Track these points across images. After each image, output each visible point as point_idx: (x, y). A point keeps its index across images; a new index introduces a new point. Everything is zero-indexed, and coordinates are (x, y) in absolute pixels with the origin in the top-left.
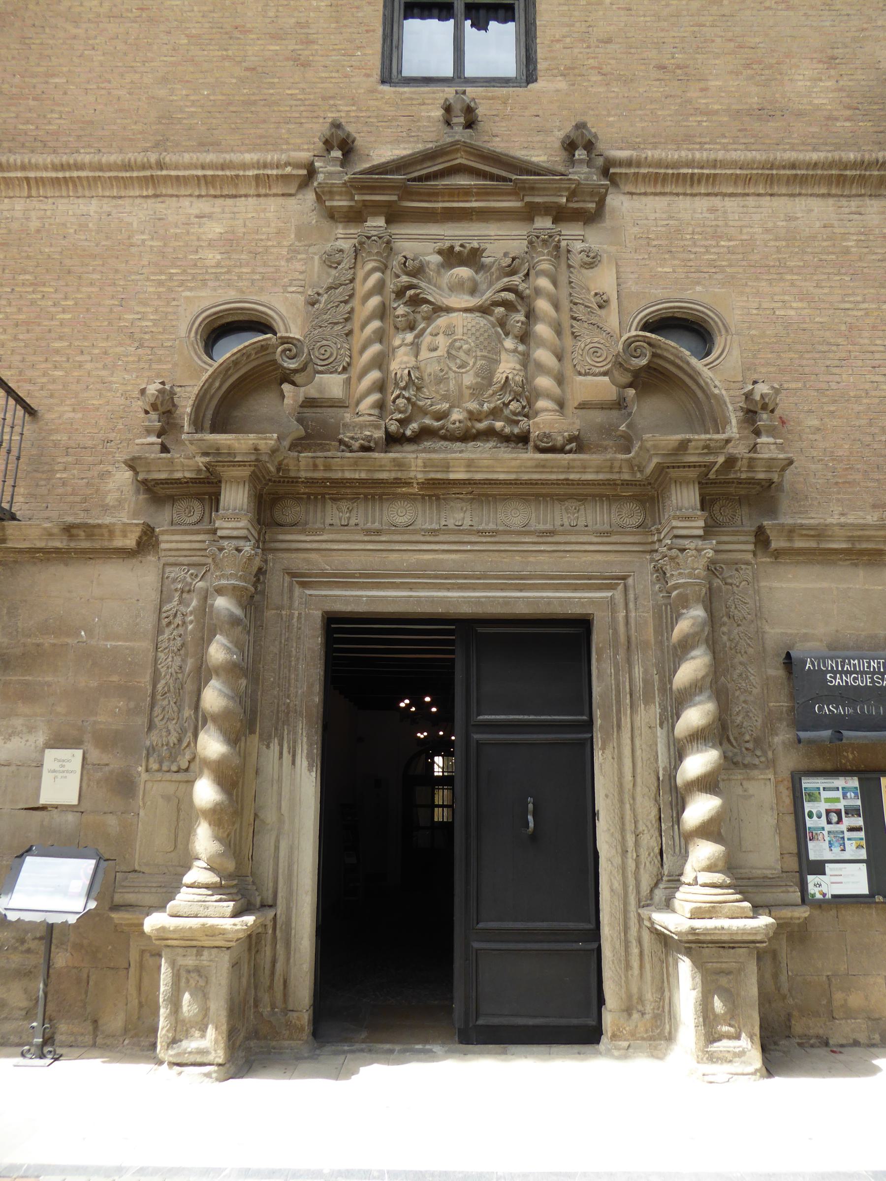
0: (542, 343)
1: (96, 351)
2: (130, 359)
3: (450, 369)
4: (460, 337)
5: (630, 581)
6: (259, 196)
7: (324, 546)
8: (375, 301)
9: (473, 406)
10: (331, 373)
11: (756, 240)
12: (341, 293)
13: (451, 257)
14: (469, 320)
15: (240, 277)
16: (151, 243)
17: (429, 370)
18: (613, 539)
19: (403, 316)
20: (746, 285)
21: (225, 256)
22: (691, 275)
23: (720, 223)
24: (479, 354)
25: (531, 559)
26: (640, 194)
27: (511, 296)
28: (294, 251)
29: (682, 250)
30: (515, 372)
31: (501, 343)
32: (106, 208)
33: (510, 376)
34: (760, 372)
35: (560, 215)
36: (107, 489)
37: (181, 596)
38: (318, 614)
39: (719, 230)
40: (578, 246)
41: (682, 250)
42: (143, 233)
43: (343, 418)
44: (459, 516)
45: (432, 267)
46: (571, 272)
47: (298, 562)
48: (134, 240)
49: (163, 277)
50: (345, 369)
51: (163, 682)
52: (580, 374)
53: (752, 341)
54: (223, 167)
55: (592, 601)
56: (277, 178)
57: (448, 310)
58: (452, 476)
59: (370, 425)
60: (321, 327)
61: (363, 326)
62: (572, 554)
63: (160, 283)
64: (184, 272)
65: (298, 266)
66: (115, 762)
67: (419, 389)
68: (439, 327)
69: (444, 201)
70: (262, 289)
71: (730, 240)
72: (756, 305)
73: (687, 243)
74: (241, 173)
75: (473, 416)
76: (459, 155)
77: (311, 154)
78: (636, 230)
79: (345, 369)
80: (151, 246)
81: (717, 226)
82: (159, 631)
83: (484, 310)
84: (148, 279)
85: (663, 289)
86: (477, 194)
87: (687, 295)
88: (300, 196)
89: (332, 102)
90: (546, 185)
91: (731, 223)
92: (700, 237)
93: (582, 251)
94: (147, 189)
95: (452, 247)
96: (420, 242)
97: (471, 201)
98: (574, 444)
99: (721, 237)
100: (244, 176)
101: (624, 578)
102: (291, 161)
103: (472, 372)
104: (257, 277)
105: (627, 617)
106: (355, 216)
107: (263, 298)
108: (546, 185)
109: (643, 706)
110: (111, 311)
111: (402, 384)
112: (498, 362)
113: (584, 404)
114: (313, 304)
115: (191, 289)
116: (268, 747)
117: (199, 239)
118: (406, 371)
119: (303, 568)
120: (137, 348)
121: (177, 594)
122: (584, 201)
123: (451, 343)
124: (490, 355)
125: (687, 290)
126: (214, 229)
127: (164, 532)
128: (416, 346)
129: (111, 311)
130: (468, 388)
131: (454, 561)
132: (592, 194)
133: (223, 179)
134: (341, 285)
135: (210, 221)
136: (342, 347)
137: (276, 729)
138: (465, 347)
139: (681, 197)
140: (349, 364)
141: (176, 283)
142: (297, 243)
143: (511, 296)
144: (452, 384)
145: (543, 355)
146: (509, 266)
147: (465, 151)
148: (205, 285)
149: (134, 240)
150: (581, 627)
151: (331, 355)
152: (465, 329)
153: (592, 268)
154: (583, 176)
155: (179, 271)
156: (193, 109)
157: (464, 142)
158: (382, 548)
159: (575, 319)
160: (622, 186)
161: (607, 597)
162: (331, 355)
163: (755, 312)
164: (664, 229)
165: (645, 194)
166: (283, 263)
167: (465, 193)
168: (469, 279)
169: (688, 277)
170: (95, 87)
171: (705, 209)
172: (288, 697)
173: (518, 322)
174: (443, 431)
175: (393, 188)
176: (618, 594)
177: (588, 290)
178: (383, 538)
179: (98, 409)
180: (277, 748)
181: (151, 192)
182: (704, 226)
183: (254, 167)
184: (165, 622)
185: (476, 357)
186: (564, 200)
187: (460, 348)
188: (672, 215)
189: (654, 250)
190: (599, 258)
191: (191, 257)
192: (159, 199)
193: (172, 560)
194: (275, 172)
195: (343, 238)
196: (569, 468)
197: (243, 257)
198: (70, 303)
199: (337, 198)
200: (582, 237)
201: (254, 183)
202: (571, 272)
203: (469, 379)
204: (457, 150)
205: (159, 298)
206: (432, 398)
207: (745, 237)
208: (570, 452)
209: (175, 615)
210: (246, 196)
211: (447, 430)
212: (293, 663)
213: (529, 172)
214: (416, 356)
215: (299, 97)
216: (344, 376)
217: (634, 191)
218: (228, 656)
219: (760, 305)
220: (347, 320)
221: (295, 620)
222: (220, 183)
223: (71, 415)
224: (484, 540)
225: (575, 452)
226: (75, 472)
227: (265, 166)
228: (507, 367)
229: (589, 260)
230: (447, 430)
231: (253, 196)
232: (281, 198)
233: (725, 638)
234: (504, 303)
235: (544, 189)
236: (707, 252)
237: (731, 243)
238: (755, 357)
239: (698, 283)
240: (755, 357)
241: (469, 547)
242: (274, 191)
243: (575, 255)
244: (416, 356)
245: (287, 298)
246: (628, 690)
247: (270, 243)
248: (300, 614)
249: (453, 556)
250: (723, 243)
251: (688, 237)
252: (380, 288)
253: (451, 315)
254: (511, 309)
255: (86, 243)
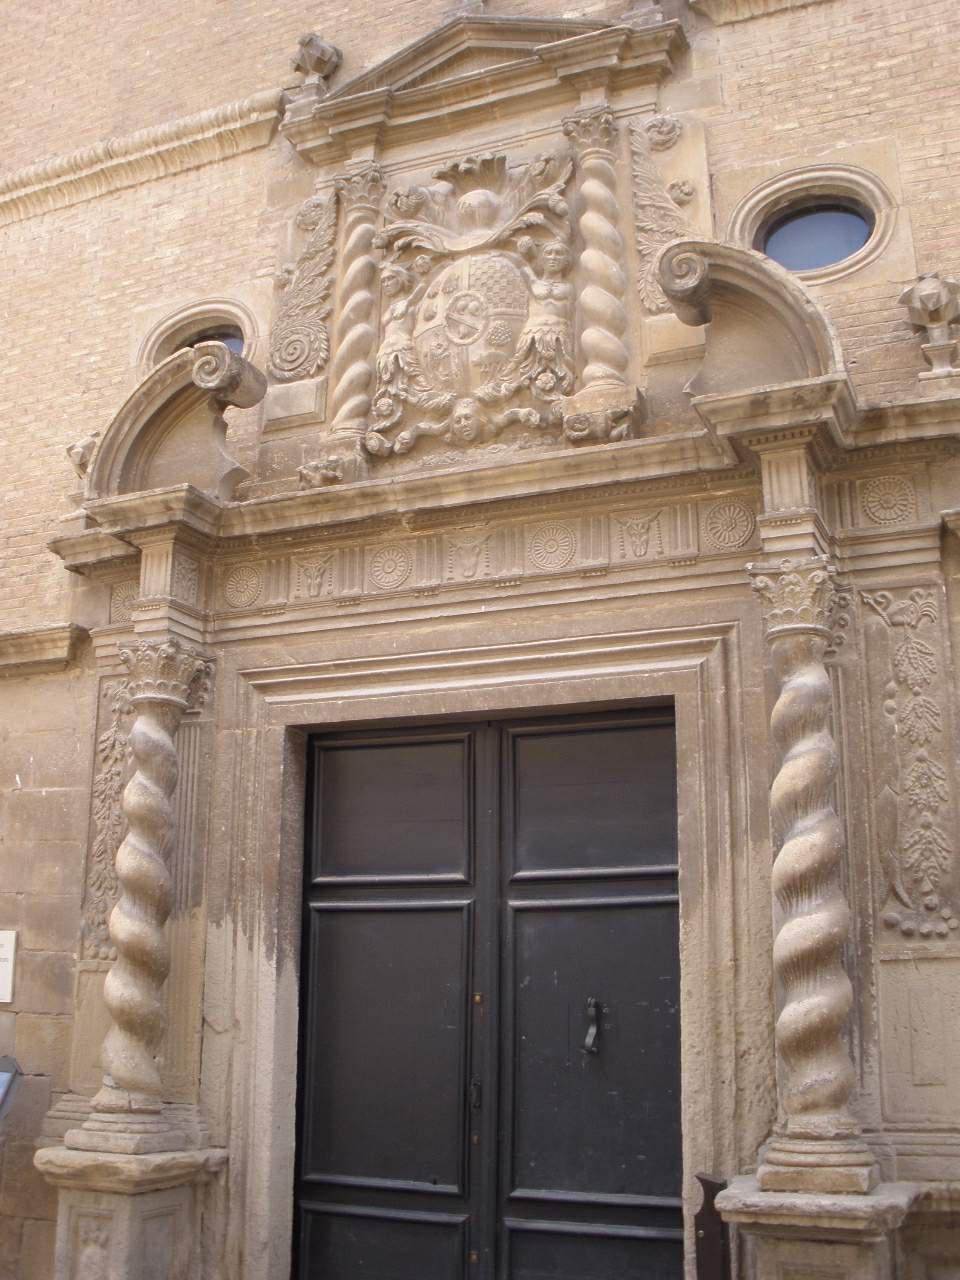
0: (592, 278)
1: (41, 407)
2: (76, 408)
3: (451, 342)
4: (464, 292)
5: (733, 636)
6: (225, 159)
7: (287, 630)
8: (359, 263)
9: (483, 390)
10: (302, 378)
11: (936, 46)
12: (320, 262)
13: (458, 177)
14: (479, 265)
15: (201, 272)
16: (103, 254)
17: (425, 349)
18: (701, 569)
19: (389, 278)
20: (921, 121)
21: (186, 247)
22: (828, 126)
23: (875, 34)
24: (492, 311)
25: (577, 616)
26: (746, 21)
27: (537, 217)
28: (265, 220)
29: (813, 90)
30: (546, 328)
31: (529, 289)
32: (58, 224)
33: (537, 338)
34: (949, 259)
35: (615, 81)
36: (46, 584)
37: (119, 720)
38: (280, 729)
39: (874, 45)
40: (648, 119)
41: (813, 90)
42: (95, 243)
43: (319, 437)
44: (471, 561)
45: (439, 199)
46: (636, 162)
47: (257, 657)
48: (86, 256)
49: (115, 294)
50: (320, 368)
51: (100, 838)
52: (650, 312)
53: (933, 209)
54: (178, 136)
55: (671, 676)
56: (243, 132)
57: (453, 256)
58: (447, 502)
59: (341, 445)
60: (290, 316)
61: (344, 300)
62: (639, 602)
63: (112, 302)
64: (138, 281)
65: (270, 239)
66: (46, 948)
67: (412, 378)
68: (438, 283)
69: (450, 105)
70: (226, 281)
71: (892, 57)
72: (938, 151)
73: (820, 77)
74: (199, 137)
75: (490, 404)
76: (465, 37)
77: (280, 88)
78: (739, 77)
79: (320, 368)
80: (104, 258)
81: (872, 39)
82: (95, 769)
83: (502, 244)
84: (99, 301)
85: (782, 156)
86: (494, 83)
87: (824, 157)
88: (274, 146)
89: (318, 11)
90: (582, 47)
91: (894, 30)
92: (843, 63)
93: (651, 127)
94: (100, 188)
95: (456, 166)
96: (416, 167)
97: (488, 94)
98: (624, 426)
99: (877, 56)
100: (204, 140)
101: (725, 630)
102: (256, 105)
103: (481, 341)
104: (221, 266)
105: (727, 696)
106: (340, 148)
107: (227, 294)
108: (582, 47)
109: (750, 844)
110: (58, 352)
111: (386, 377)
112: (522, 318)
113: (658, 359)
114: (283, 286)
115: (145, 302)
116: (219, 925)
117: (157, 234)
118: (392, 357)
119: (265, 664)
120: (84, 392)
121: (115, 717)
122: (648, 54)
123: (453, 304)
124: (511, 310)
125: (822, 149)
126: (174, 216)
127: (101, 634)
128: (409, 319)
129: (58, 352)
130: (478, 364)
131: (463, 632)
132: (656, 41)
133: (182, 150)
134: (317, 252)
135: (163, 210)
136: (316, 339)
137: (229, 900)
138: (472, 305)
139: (810, 9)
140: (326, 361)
141: (128, 299)
142: (270, 209)
143: (537, 217)
144: (454, 362)
145: (593, 297)
146: (541, 173)
147: (473, 30)
148: (160, 292)
149: (86, 256)
150: (658, 713)
151: (302, 352)
152: (473, 279)
153: (668, 148)
154: (640, 20)
155: (132, 281)
156: (156, 72)
157: (467, 18)
158: (363, 623)
159: (641, 229)
160: (714, 17)
161: (695, 666)
162: (302, 352)
163: (937, 162)
164: (784, 65)
165: (753, 18)
166: (252, 240)
167: (477, 86)
168: (481, 205)
169: (823, 131)
170: (796, 125)
171: (849, 19)
172: (244, 854)
173: (550, 253)
174: (448, 435)
175: (375, 105)
176: (714, 658)
177: (660, 182)
178: (362, 609)
179: (39, 482)
180: (230, 926)
181: (104, 190)
182: (849, 45)
183: (213, 126)
184: (101, 756)
185: (487, 318)
186: (614, 61)
187: (464, 308)
188: (798, 39)
189: (767, 100)
190: (678, 131)
191: (148, 259)
192: (116, 195)
193: (108, 671)
194: (238, 125)
195: (321, 186)
196: (615, 463)
197: (206, 243)
198: (17, 351)
199: (310, 136)
200: (653, 107)
201: (217, 145)
202: (636, 162)
203: (478, 352)
204: (461, 32)
205: (110, 321)
206: (427, 392)
207: (919, 45)
208: (619, 438)
209: (113, 746)
210: (211, 163)
211: (454, 434)
212: (250, 804)
213: (560, 35)
214: (411, 332)
215: (280, 16)
216: (320, 379)
217: (734, 19)
218: (142, 799)
219: (945, 149)
220: (325, 298)
221: (253, 741)
222: (175, 157)
223: (12, 495)
224: (503, 594)
225: (628, 437)
226: (14, 568)
227: (226, 121)
228: (540, 323)
229: (662, 137)
230: (454, 434)
231: (219, 161)
232: (251, 155)
233: (892, 718)
234: (530, 228)
235: (582, 53)
236: (855, 83)
237: (895, 61)
238: (937, 236)
239: (840, 136)
240: (937, 236)
241: (483, 609)
242: (242, 147)
243: (640, 135)
244: (411, 332)
245: (254, 286)
246: (727, 818)
247: (238, 218)
248: (259, 732)
249: (462, 625)
250: (880, 64)
251: (823, 67)
252: (365, 246)
253: (457, 263)
254: (545, 237)
255: (36, 273)
